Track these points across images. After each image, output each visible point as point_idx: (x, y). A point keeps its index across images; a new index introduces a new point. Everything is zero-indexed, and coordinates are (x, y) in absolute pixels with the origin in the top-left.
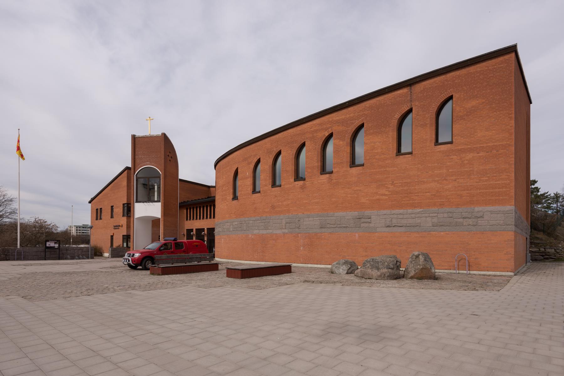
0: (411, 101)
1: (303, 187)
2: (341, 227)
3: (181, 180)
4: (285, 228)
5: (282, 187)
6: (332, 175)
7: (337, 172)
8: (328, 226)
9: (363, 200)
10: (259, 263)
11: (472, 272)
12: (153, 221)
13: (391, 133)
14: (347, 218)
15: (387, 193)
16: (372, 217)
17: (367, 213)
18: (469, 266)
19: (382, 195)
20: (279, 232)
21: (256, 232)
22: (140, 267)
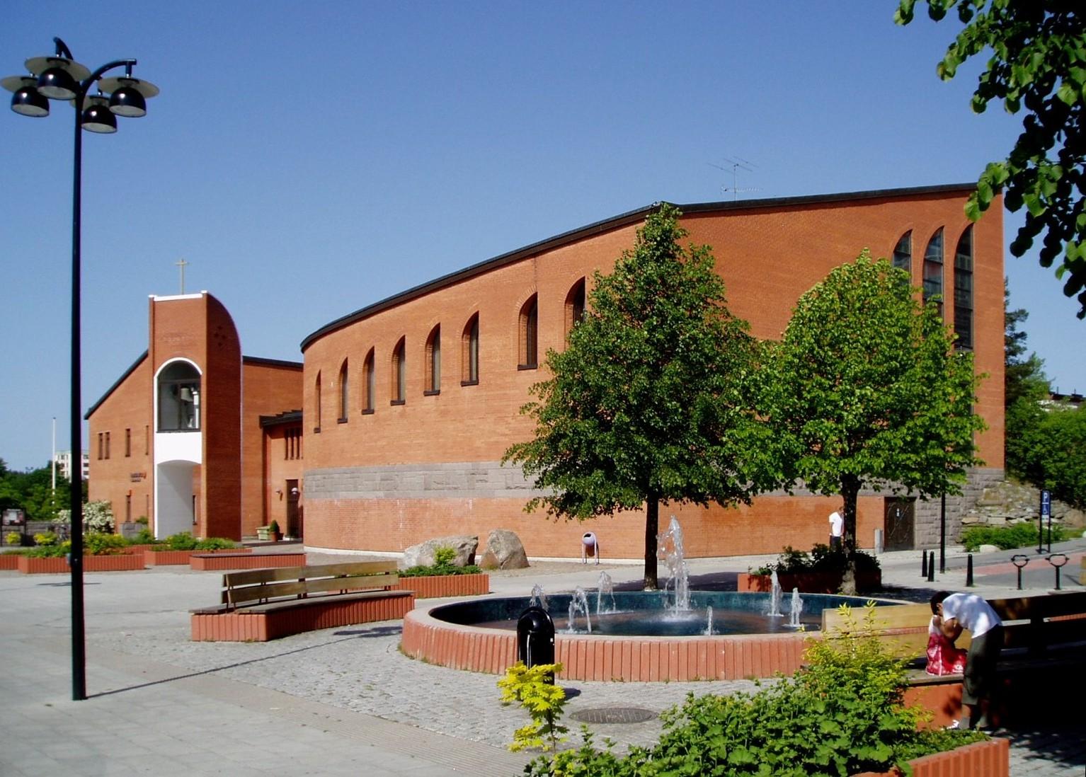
0: (536, 281)
1: (402, 415)
2: (449, 489)
3: (251, 361)
4: (380, 490)
5: (375, 413)
6: (440, 397)
7: (446, 392)
8: (434, 486)
9: (478, 443)
10: (352, 552)
11: (601, 561)
12: (17, 568)
13: (512, 332)
14: (459, 472)
15: (507, 432)
16: (489, 471)
17: (484, 464)
18: (78, 548)
19: (502, 435)
20: (372, 496)
21: (343, 494)
22: (1004, 730)
